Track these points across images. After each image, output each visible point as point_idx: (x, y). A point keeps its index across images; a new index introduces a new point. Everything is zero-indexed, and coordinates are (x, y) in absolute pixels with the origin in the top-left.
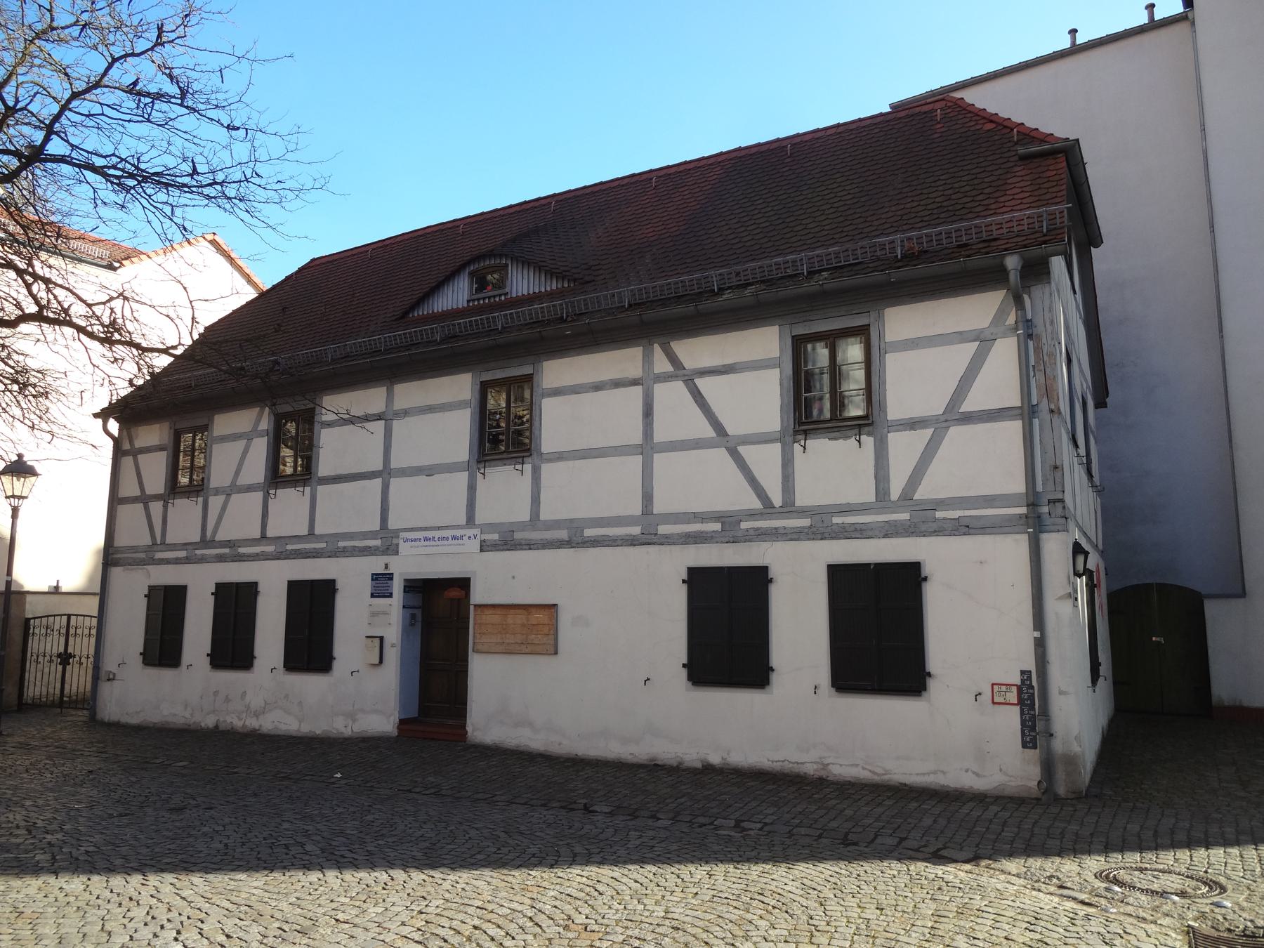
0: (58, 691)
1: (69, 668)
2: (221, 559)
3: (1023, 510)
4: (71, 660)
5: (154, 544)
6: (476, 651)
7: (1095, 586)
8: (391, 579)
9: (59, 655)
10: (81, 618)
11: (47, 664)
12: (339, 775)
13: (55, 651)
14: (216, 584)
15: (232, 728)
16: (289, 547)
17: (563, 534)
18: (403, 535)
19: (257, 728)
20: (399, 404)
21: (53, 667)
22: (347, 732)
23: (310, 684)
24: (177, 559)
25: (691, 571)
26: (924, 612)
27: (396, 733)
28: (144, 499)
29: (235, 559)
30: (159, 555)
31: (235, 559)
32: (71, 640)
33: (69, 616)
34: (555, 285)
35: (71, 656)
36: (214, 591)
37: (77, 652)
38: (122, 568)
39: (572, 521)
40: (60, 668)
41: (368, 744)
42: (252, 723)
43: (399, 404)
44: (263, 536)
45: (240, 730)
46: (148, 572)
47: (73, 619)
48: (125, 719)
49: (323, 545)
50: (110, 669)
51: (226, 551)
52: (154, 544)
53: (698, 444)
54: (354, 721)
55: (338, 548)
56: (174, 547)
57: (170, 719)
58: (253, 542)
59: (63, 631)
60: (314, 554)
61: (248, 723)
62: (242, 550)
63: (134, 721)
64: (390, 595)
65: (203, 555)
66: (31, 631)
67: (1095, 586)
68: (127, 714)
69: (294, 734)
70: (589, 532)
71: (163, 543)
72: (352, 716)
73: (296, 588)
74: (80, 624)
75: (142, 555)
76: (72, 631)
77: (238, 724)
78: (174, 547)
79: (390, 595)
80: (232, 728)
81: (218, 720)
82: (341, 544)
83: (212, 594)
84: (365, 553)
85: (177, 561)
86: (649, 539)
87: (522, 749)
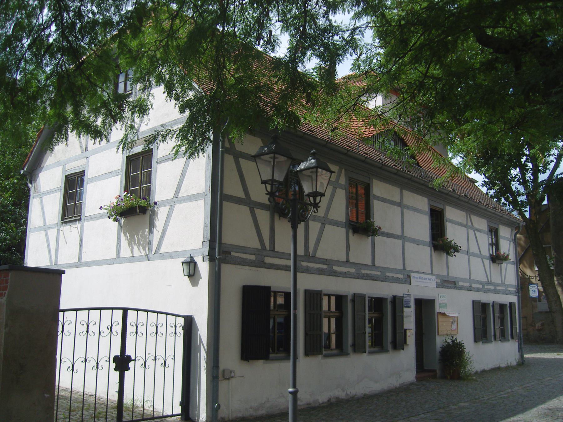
0: (114, 397)
1: (128, 375)
2: (321, 272)
4: (131, 365)
7: (494, 244)
9: (116, 359)
10: (142, 315)
16: (363, 271)
20: (485, 260)
21: (103, 373)
26: (241, 307)
27: (415, 380)
30: (268, 260)
33: (125, 311)
34: (428, 32)
35: (129, 359)
36: (63, 275)
41: (405, 389)
43: (485, 260)
44: (348, 261)
49: (379, 273)
51: (325, 267)
55: (507, 290)
60: (376, 278)
61: (348, 393)
62: (336, 268)
65: (308, 267)
67: (494, 244)
71: (273, 249)
82: (388, 274)
84: (397, 282)
86: (470, 289)
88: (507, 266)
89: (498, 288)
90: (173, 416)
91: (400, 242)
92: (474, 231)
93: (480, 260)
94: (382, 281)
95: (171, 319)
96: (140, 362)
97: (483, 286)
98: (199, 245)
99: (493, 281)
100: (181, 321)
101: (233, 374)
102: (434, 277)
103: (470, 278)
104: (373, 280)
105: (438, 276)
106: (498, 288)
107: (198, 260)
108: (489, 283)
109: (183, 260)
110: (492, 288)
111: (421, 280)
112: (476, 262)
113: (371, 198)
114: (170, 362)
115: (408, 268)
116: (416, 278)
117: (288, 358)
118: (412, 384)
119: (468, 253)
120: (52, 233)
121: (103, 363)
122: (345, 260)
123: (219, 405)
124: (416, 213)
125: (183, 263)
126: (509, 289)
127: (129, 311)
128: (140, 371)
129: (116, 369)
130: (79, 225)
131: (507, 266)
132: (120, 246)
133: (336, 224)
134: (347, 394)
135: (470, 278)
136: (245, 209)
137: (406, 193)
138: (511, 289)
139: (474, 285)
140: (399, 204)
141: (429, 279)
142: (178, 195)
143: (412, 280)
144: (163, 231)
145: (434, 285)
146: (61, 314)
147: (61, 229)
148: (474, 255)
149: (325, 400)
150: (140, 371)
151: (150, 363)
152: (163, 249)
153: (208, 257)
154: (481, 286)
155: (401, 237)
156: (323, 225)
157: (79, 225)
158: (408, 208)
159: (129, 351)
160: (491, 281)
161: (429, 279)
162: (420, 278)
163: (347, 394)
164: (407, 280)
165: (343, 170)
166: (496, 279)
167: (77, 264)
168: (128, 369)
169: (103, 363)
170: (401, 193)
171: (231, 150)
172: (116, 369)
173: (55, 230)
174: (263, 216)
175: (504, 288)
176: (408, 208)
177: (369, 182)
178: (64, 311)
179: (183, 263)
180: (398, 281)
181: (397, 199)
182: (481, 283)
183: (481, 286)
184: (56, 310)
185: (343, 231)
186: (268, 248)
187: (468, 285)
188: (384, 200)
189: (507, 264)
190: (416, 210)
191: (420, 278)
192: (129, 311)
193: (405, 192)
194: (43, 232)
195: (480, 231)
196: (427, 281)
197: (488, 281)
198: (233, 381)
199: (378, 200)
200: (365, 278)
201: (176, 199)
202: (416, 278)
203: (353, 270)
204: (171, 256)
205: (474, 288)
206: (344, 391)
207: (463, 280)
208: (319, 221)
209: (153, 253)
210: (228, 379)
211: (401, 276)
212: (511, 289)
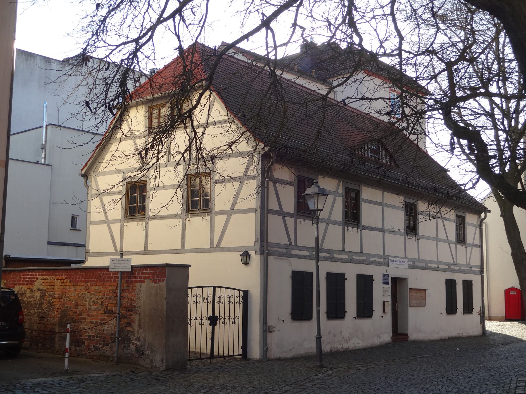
1: (216, 327)
3: (479, 269)
4: (218, 322)
5: (291, 244)
6: (410, 306)
8: (388, 277)
9: (210, 318)
11: (232, 325)
12: (457, 349)
13: (204, 315)
14: (446, 280)
15: (337, 350)
16: (354, 257)
17: (423, 265)
18: (390, 258)
19: (348, 348)
21: (204, 327)
22: (378, 343)
23: (365, 323)
24: (304, 256)
25: (312, 273)
27: (391, 341)
28: (284, 215)
29: (332, 260)
30: (294, 252)
31: (332, 260)
32: (217, 306)
33: (214, 288)
37: (222, 315)
38: (273, 257)
39: (425, 260)
40: (210, 328)
41: (384, 347)
42: (346, 346)
44: (344, 250)
45: (340, 350)
46: (290, 262)
47: (217, 289)
48: (283, 356)
49: (365, 258)
50: (270, 325)
51: (328, 255)
52: (291, 244)
53: (234, 204)
54: (380, 338)
55: (472, 270)
56: (301, 248)
57: (310, 351)
58: (339, 252)
59: (211, 299)
61: (344, 346)
62: (336, 256)
63: (290, 355)
64: (388, 284)
66: (241, 300)
68: (284, 352)
69: (361, 348)
70: (429, 265)
71: (296, 245)
72: (379, 336)
73: (330, 276)
74: (223, 293)
75: (284, 250)
76: (217, 299)
77: (340, 347)
78: (301, 248)
79: (388, 284)
80: (337, 350)
81: (331, 347)
82: (372, 259)
83: (374, 280)
85: (304, 257)
86: (437, 269)
87: (374, 346)
88: (472, 249)
89: (463, 268)
90: (238, 355)
91: (381, 233)
92: (443, 220)
93: (447, 244)
94: (368, 264)
95: (237, 292)
96: (222, 320)
97: (449, 267)
98: (252, 244)
99: (458, 262)
100: (241, 293)
101: (274, 329)
102: (407, 260)
103: (438, 261)
104: (361, 263)
105: (410, 259)
106: (463, 268)
107: (252, 253)
108: (455, 264)
109: (241, 253)
110: (458, 268)
111: (397, 263)
112: (444, 247)
113: (361, 201)
114: (237, 320)
115: (387, 253)
116: (392, 261)
117: (310, 318)
118: (389, 343)
119: (437, 239)
120: (116, 228)
121: (204, 321)
122: (341, 249)
123: (267, 348)
124: (394, 210)
125: (241, 255)
126: (473, 269)
127: (216, 288)
128: (222, 326)
129: (210, 325)
130: (144, 223)
131: (472, 249)
132: (185, 240)
133: (336, 223)
134: (342, 347)
135: (438, 261)
136: (280, 218)
137: (387, 194)
138: (475, 269)
139: (441, 266)
140: (380, 204)
141: (403, 262)
142: (234, 208)
143: (390, 263)
144: (222, 232)
145: (407, 266)
146: (189, 290)
147: (125, 224)
148: (442, 241)
149: (329, 350)
150: (222, 326)
151: (227, 321)
152: (222, 245)
153: (259, 252)
154: (447, 267)
155: (382, 230)
156: (328, 224)
157: (144, 223)
158: (387, 206)
159: (217, 314)
160: (456, 263)
161: (403, 262)
162: (396, 261)
163: (342, 347)
164: (386, 264)
165: (341, 182)
166: (461, 260)
167: (143, 252)
168: (216, 324)
169: (204, 321)
170: (383, 194)
171: (271, 179)
172: (210, 325)
173: (119, 225)
174: (453, 246)
175: (469, 269)
176: (387, 206)
177: (358, 189)
178: (191, 288)
179: (241, 255)
180: (378, 264)
181: (379, 200)
182: (447, 264)
183: (447, 267)
184: (187, 288)
185: (340, 228)
186: (293, 244)
187: (436, 266)
188: (370, 202)
189: (472, 247)
190: (394, 207)
191: (396, 261)
192: (216, 288)
193: (385, 193)
194: (106, 225)
195: (447, 220)
196: (402, 263)
197: (454, 263)
198: (274, 333)
199: (365, 202)
200: (355, 262)
201: (232, 211)
202: (392, 261)
203: (346, 257)
204: (230, 250)
205: (441, 269)
206: (340, 345)
207: (432, 262)
208: (325, 222)
209: (215, 247)
210: (271, 332)
211: (381, 260)
212: (475, 269)
